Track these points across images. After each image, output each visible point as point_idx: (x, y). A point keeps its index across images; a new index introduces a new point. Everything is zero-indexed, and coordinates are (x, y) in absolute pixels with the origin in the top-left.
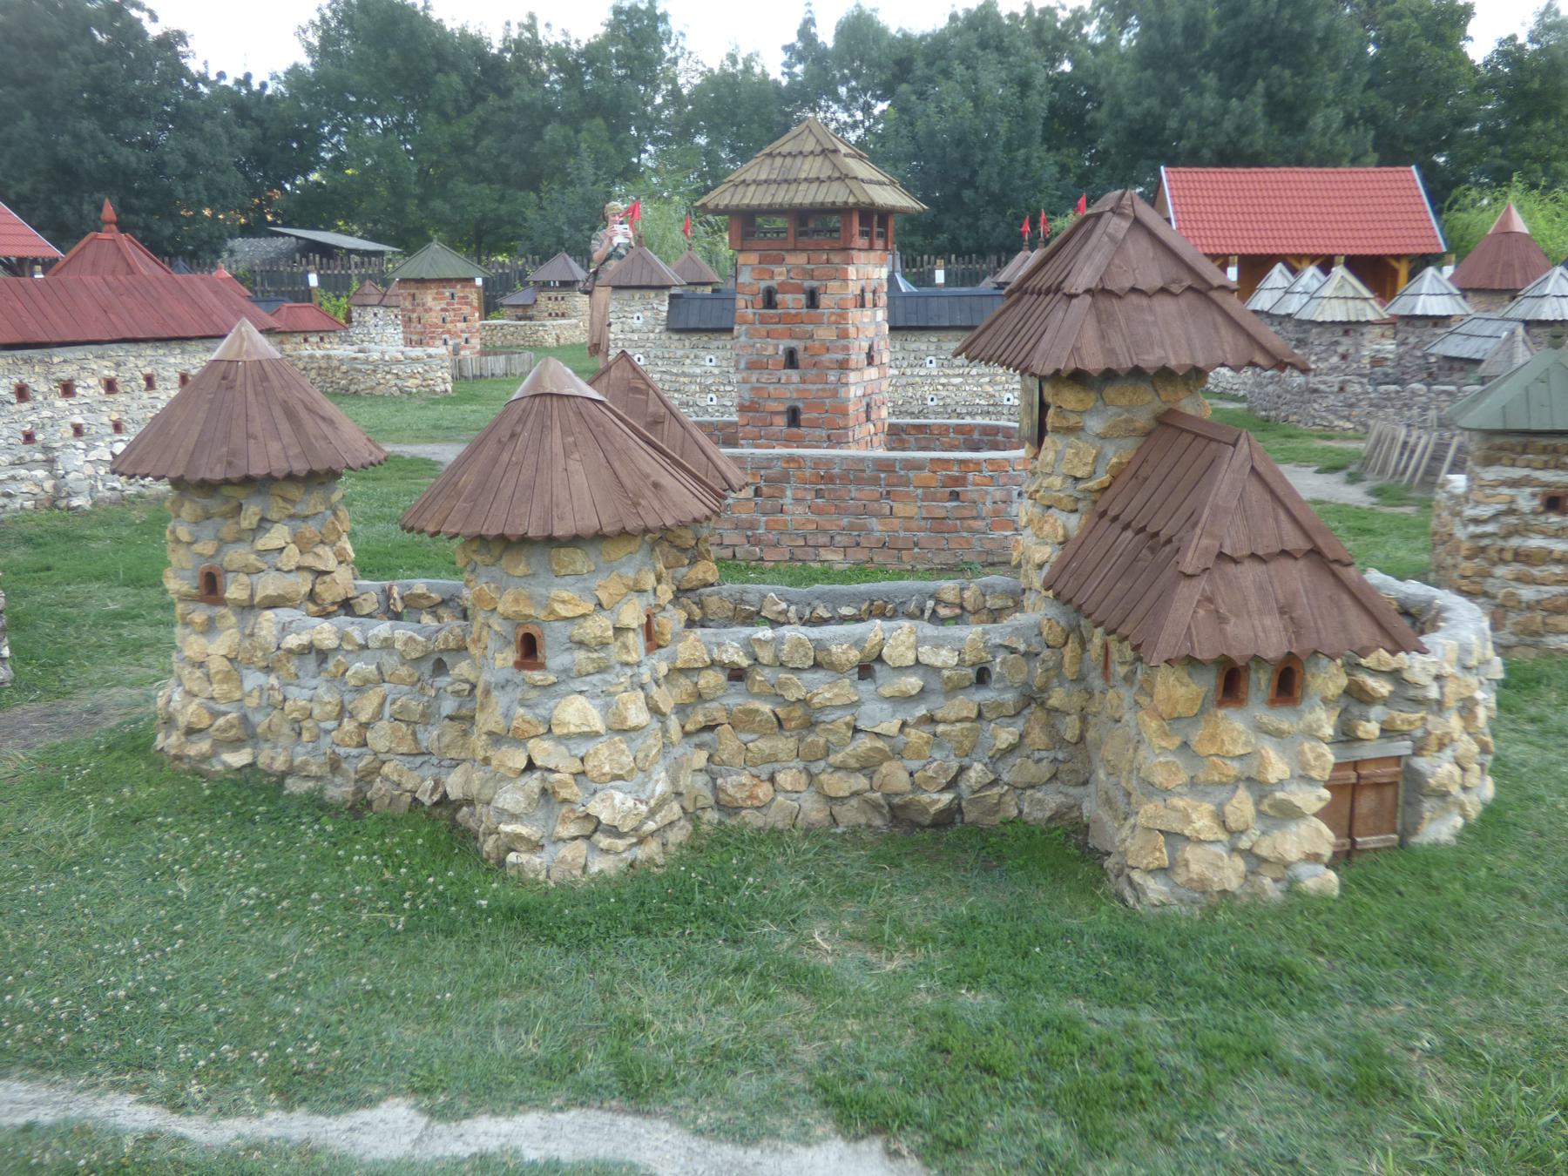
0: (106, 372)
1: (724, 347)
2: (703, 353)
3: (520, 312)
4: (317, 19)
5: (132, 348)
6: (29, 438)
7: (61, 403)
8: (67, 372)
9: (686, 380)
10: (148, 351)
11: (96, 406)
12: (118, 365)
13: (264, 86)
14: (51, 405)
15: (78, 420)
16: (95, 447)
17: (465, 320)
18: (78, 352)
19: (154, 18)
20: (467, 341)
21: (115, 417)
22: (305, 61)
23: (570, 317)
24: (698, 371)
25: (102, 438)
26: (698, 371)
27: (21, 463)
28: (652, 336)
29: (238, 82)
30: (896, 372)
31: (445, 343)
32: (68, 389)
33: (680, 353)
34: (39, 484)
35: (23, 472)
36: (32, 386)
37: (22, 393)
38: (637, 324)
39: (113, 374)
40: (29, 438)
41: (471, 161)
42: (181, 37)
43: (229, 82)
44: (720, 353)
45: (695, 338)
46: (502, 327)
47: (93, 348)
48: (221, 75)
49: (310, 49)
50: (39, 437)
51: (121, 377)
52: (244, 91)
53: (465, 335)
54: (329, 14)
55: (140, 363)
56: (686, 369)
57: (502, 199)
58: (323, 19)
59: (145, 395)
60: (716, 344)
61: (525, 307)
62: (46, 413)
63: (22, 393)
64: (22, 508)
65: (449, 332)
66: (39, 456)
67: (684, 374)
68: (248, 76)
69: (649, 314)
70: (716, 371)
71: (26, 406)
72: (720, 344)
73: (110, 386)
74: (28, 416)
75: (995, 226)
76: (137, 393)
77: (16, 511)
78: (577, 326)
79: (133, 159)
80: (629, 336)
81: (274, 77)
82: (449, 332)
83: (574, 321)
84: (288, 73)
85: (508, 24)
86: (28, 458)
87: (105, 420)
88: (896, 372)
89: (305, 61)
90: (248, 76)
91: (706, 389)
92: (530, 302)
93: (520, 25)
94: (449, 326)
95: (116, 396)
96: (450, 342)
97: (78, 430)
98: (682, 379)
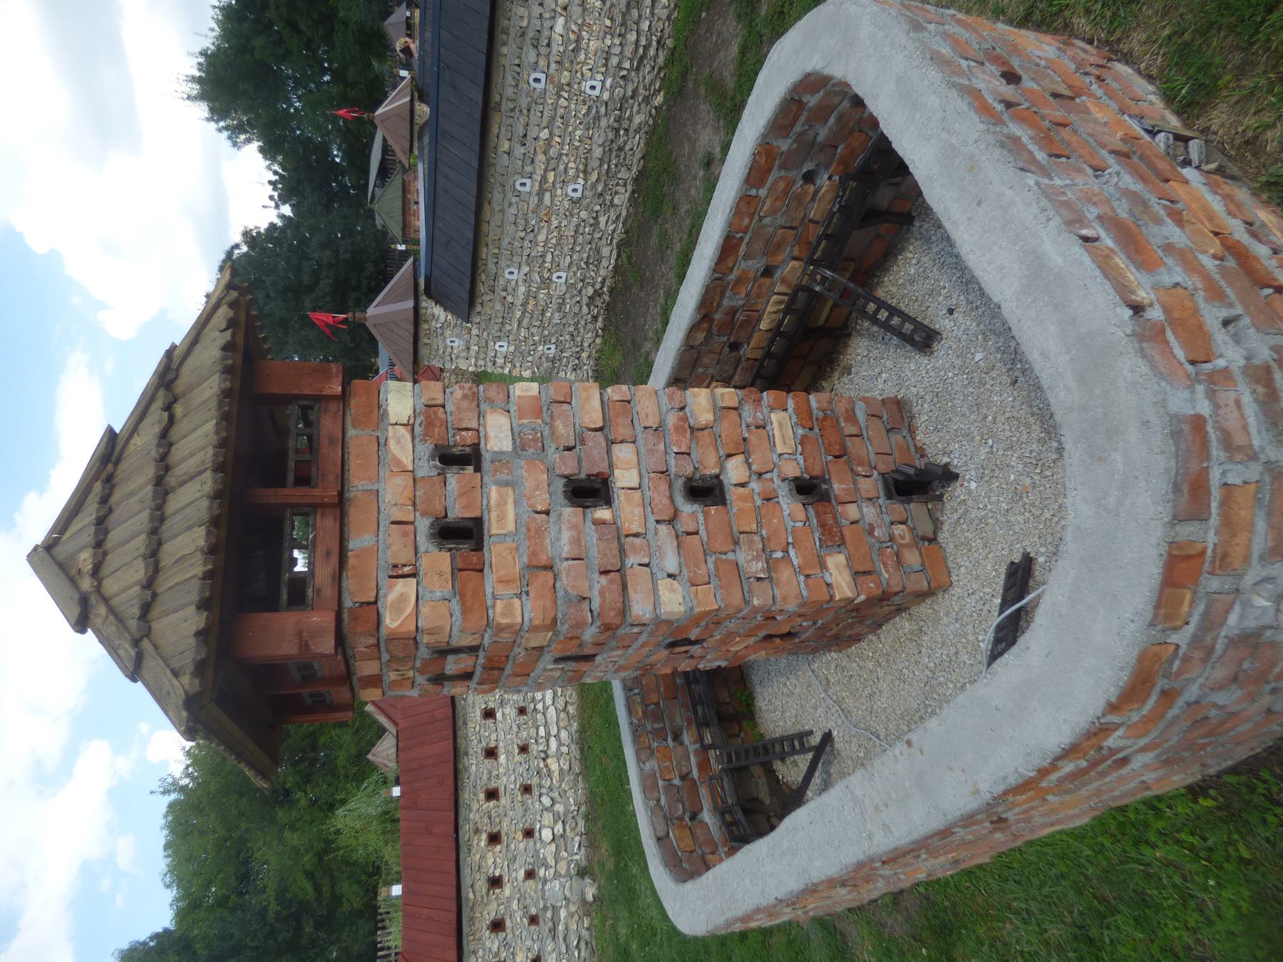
0: (483, 844)
1: (496, 256)
2: (502, 282)
4: (226, 134)
5: (463, 812)
6: (534, 920)
7: (507, 891)
8: (482, 885)
9: (532, 302)
10: (466, 796)
11: (510, 856)
12: (477, 831)
13: (275, 173)
14: (509, 899)
15: (522, 874)
16: (545, 858)
18: (466, 872)
19: (237, 246)
21: (519, 835)
22: (256, 145)
24: (522, 289)
25: (537, 851)
26: (522, 289)
27: (553, 930)
28: (475, 332)
29: (275, 189)
30: (561, 21)
32: (496, 882)
33: (498, 306)
34: (571, 915)
35: (561, 927)
36: (492, 917)
37: (497, 926)
38: (458, 344)
39: (484, 836)
40: (534, 920)
42: (246, 234)
43: (276, 194)
44: (503, 263)
45: (481, 288)
47: (462, 857)
48: (271, 198)
49: (249, 141)
50: (533, 911)
51: (487, 828)
54: (222, 124)
55: (475, 806)
56: (518, 302)
58: (226, 128)
59: (503, 801)
60: (491, 266)
62: (515, 905)
63: (497, 926)
64: (588, 929)
66: (549, 914)
67: (525, 304)
68: (270, 182)
69: (448, 332)
70: (526, 269)
71: (508, 923)
72: (491, 261)
73: (494, 839)
74: (516, 921)
76: (501, 810)
77: (591, 935)
79: (327, 281)
80: (473, 354)
81: (269, 167)
84: (265, 158)
86: (550, 924)
87: (522, 846)
88: (561, 21)
89: (256, 145)
90: (270, 182)
91: (546, 283)
95: (503, 833)
97: (530, 875)
98: (530, 307)
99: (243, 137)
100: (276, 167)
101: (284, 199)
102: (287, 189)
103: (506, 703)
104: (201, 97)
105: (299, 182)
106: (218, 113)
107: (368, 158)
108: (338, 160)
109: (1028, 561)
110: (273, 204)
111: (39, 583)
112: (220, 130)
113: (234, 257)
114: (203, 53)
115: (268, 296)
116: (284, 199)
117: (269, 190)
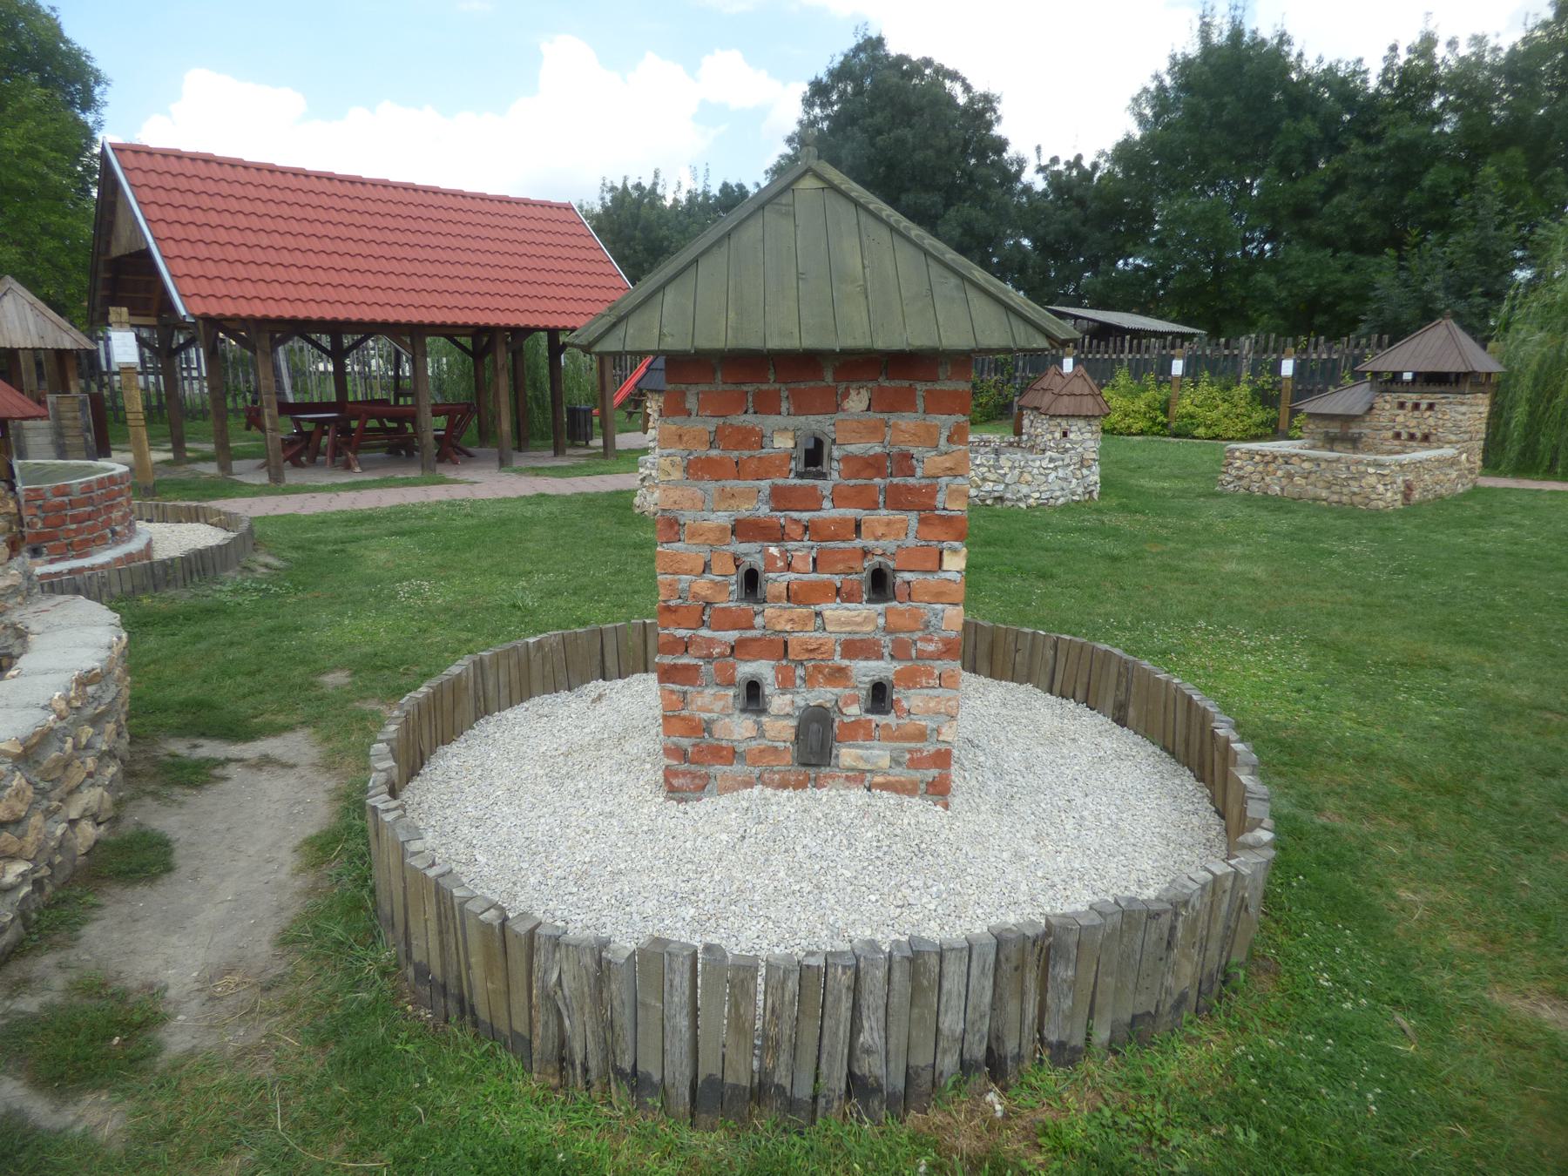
3: (1334, 429)
4: (1152, 86)
13: (1095, 166)
17: (880, 585)
20: (880, 696)
23: (1441, 443)
29: (1070, 166)
31: (753, 693)
41: (1314, 226)
43: (1061, 167)
46: (1287, 460)
48: (1055, 160)
52: (1075, 173)
53: (866, 670)
54: (1168, 81)
57: (1348, 269)
61: (1347, 419)
65: (780, 649)
68: (1079, 158)
75: (298, 373)
78: (1453, 462)
81: (1102, 154)
82: (780, 649)
83: (1448, 452)
85: (1394, 48)
90: (1079, 158)
92: (1358, 410)
93: (1410, 50)
94: (774, 616)
96: (779, 702)
99: (1148, 112)
100: (1105, 166)
101: (1055, 180)
102: (1071, 186)
103: (1487, 402)
104: (1208, 49)
105: (1081, 202)
106: (1184, 69)
107: (1126, 309)
108: (1121, 263)
109: (819, 443)
110: (1045, 161)
111: (492, 190)
112: (1157, 77)
113: (948, 83)
114: (1283, 39)
115: (879, 132)
116: (1055, 180)
117: (1067, 156)
